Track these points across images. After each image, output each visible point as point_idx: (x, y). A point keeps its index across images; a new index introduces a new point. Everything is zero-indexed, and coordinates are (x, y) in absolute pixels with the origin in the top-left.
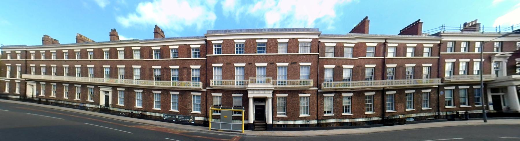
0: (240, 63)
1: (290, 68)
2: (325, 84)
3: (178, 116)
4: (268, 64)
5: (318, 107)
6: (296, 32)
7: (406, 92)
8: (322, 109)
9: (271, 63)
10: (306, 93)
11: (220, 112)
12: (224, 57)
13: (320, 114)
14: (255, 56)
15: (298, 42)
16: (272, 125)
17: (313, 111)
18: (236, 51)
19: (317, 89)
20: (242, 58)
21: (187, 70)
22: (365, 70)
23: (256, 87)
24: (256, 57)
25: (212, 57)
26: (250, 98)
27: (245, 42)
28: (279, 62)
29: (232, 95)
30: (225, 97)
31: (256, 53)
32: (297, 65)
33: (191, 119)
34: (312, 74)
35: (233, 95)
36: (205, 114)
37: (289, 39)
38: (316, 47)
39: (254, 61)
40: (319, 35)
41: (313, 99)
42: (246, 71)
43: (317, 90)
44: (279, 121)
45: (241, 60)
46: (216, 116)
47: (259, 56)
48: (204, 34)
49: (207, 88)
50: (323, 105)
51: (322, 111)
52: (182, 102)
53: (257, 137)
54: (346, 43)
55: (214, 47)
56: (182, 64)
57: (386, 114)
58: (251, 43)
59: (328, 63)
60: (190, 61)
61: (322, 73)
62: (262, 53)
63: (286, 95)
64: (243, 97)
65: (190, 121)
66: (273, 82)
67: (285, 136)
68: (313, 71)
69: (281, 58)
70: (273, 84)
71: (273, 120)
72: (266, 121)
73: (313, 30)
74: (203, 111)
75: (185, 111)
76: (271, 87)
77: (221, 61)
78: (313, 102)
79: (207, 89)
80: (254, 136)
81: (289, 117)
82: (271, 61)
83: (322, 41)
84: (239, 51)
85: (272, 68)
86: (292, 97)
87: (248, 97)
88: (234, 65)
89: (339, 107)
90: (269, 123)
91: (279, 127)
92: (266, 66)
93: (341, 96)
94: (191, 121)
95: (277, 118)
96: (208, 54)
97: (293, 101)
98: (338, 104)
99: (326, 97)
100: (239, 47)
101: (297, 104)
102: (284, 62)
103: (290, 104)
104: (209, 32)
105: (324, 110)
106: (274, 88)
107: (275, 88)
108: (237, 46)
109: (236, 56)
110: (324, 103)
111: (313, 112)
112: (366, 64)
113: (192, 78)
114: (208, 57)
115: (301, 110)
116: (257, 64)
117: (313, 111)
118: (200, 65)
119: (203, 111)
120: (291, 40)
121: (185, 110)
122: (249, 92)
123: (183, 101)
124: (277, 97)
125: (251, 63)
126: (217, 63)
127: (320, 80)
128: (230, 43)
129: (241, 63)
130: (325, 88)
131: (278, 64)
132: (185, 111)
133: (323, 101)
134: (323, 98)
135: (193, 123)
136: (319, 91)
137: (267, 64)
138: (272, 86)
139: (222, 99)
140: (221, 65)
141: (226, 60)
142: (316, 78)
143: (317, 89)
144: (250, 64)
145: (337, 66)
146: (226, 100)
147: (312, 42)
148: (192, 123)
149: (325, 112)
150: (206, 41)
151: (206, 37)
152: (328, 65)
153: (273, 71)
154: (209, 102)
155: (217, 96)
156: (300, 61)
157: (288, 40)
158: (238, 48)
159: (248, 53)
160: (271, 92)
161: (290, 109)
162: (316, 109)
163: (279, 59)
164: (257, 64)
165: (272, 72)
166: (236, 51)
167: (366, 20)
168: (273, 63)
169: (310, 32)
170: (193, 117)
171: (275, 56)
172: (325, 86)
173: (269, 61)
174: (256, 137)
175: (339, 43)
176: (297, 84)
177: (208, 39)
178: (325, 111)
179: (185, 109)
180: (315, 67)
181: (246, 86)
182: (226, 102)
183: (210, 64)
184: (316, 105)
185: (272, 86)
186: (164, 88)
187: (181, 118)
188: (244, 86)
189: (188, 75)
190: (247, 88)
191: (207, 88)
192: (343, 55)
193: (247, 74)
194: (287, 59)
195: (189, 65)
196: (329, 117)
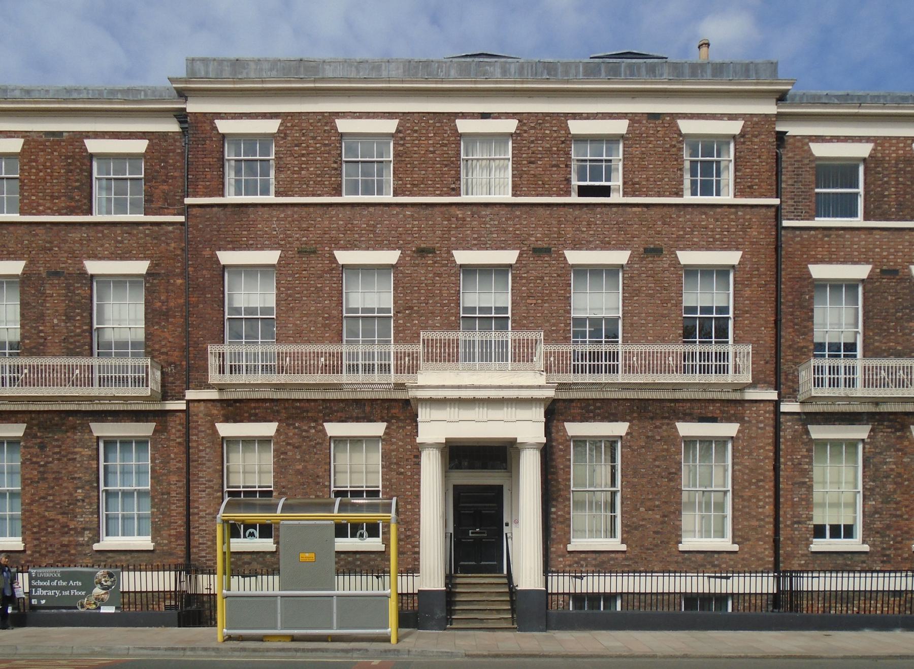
0: (367, 249)
1: (639, 275)
2: (819, 370)
3: (31, 578)
4: (520, 255)
5: (782, 500)
6: (670, 82)
8: (804, 514)
9: (538, 251)
10: (713, 420)
11: (266, 531)
12: (289, 211)
13: (792, 539)
14: (453, 210)
15: (680, 134)
16: (545, 595)
17: (755, 523)
19: (773, 395)
20: (381, 223)
21: (67, 287)
23: (459, 387)
24: (459, 213)
25: (215, 209)
26: (424, 445)
27: (398, 131)
28: (577, 245)
29: (323, 431)
30: (295, 440)
32: (665, 262)
33: (98, 591)
34: (747, 312)
35: (333, 429)
36: (180, 551)
37: (633, 118)
38: (764, 164)
39: (449, 239)
40: (781, 97)
41: (750, 453)
42: (405, 295)
43: (777, 404)
44: (581, 578)
45: (372, 229)
46: (247, 558)
47: (475, 209)
48: (172, 80)
49: (191, 395)
50: (810, 488)
51: (804, 523)
52: (43, 485)
53: (466, 659)
55: (229, 155)
56: (45, 249)
58: (428, 138)
59: (831, 253)
60: (84, 233)
61: (802, 307)
63: (620, 429)
64: (386, 438)
65: (93, 600)
66: (547, 355)
67: (611, 657)
68: (748, 299)
69: (589, 224)
70: (548, 369)
71: (547, 570)
72: (509, 576)
73: (747, 70)
74: (165, 533)
75: (65, 540)
76: (540, 387)
77: (269, 239)
78: (751, 470)
79: (188, 402)
80: (451, 655)
81: (637, 551)
82: (538, 237)
83: (793, 130)
85: (542, 278)
86: (653, 437)
87: (419, 440)
88: (333, 259)
89: (897, 503)
90: (524, 588)
91: (582, 608)
92: (510, 266)
93: (906, 443)
94: (100, 602)
95: (569, 559)
96: (195, 195)
97: (655, 460)
98: (890, 487)
99: (823, 443)
101: (670, 480)
102: (605, 245)
103: (643, 476)
104: (199, 66)
105: (811, 519)
106: (551, 393)
107: (561, 387)
109: (348, 211)
110: (811, 479)
111: (754, 529)
114: (194, 211)
115: (690, 520)
116: (462, 257)
117: (755, 523)
118: (144, 258)
119: (165, 533)
120: (639, 122)
121: (64, 534)
122: (423, 414)
123: (50, 476)
124: (568, 439)
125: (432, 251)
126: (248, 247)
127: (790, 347)
128: (314, 138)
129: (374, 249)
130: (816, 392)
131: (574, 257)
132: (65, 540)
133: (810, 463)
134: (810, 450)
135: (111, 610)
136: (785, 407)
137: (516, 253)
138: (541, 380)
139: (278, 453)
140: (271, 257)
141: (301, 229)
142: (767, 334)
143: (773, 395)
144: (422, 252)
145: (882, 271)
146: (303, 460)
147: (743, 134)
148: (105, 610)
149: (819, 531)
150: (181, 116)
151: (183, 94)
152: (830, 262)
153: (550, 295)
154: (204, 474)
155: (248, 441)
157: (20, 142)
158: (697, 162)
159: (412, 194)
160: (538, 414)
161: (642, 509)
162: (769, 509)
163: (578, 229)
164: (462, 257)
165: (544, 301)
168: (548, 251)
169: (730, 82)
170: (110, 575)
171: (562, 211)
172: (818, 383)
173: (530, 235)
174: (458, 659)
175: (890, 138)
176: (668, 370)
177: (193, 107)
178: (817, 521)
179: (65, 530)
180: (759, 276)
181: (404, 378)
182: (299, 472)
183: (207, 253)
184: (770, 485)
185: (541, 380)
187: (44, 588)
188: (393, 378)
189: (69, 318)
190: (412, 394)
191: (191, 395)
193: (411, 308)
194: (620, 229)
195: (78, 258)
196: (840, 561)
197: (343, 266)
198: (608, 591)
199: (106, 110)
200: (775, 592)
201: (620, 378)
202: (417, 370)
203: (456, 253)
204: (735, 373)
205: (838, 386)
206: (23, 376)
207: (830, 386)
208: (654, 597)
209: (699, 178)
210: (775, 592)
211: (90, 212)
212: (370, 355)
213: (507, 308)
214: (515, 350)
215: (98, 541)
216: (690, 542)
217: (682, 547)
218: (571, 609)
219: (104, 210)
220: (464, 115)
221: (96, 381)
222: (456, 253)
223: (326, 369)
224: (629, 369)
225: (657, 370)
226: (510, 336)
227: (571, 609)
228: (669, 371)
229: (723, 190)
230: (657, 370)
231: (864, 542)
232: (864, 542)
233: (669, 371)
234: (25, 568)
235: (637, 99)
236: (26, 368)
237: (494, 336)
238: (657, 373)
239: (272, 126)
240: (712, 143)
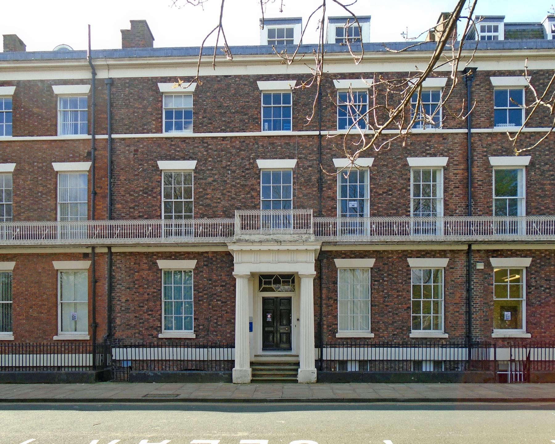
37: (299, 78)
54: (173, 79)
102: (283, 157)
107: (323, 244)
157: (293, 83)
198: (416, 359)
199: (49, 67)
200: (467, 359)
202: (233, 234)
203: (54, 164)
204: (445, 234)
206: (17, 233)
208: (202, 363)
210: (467, 359)
211: (56, 135)
212: (180, 226)
214: (289, 222)
215: (57, 334)
218: (443, 370)
219: (289, 128)
220: (343, 76)
221: (183, 233)
222: (54, 164)
223: (151, 236)
225: (141, 236)
226: (292, 212)
227: (443, 370)
230: (141, 236)
231: (445, 332)
232: (445, 332)
234: (547, 346)
235: (82, 71)
237: (281, 213)
238: (141, 237)
239: (365, 84)
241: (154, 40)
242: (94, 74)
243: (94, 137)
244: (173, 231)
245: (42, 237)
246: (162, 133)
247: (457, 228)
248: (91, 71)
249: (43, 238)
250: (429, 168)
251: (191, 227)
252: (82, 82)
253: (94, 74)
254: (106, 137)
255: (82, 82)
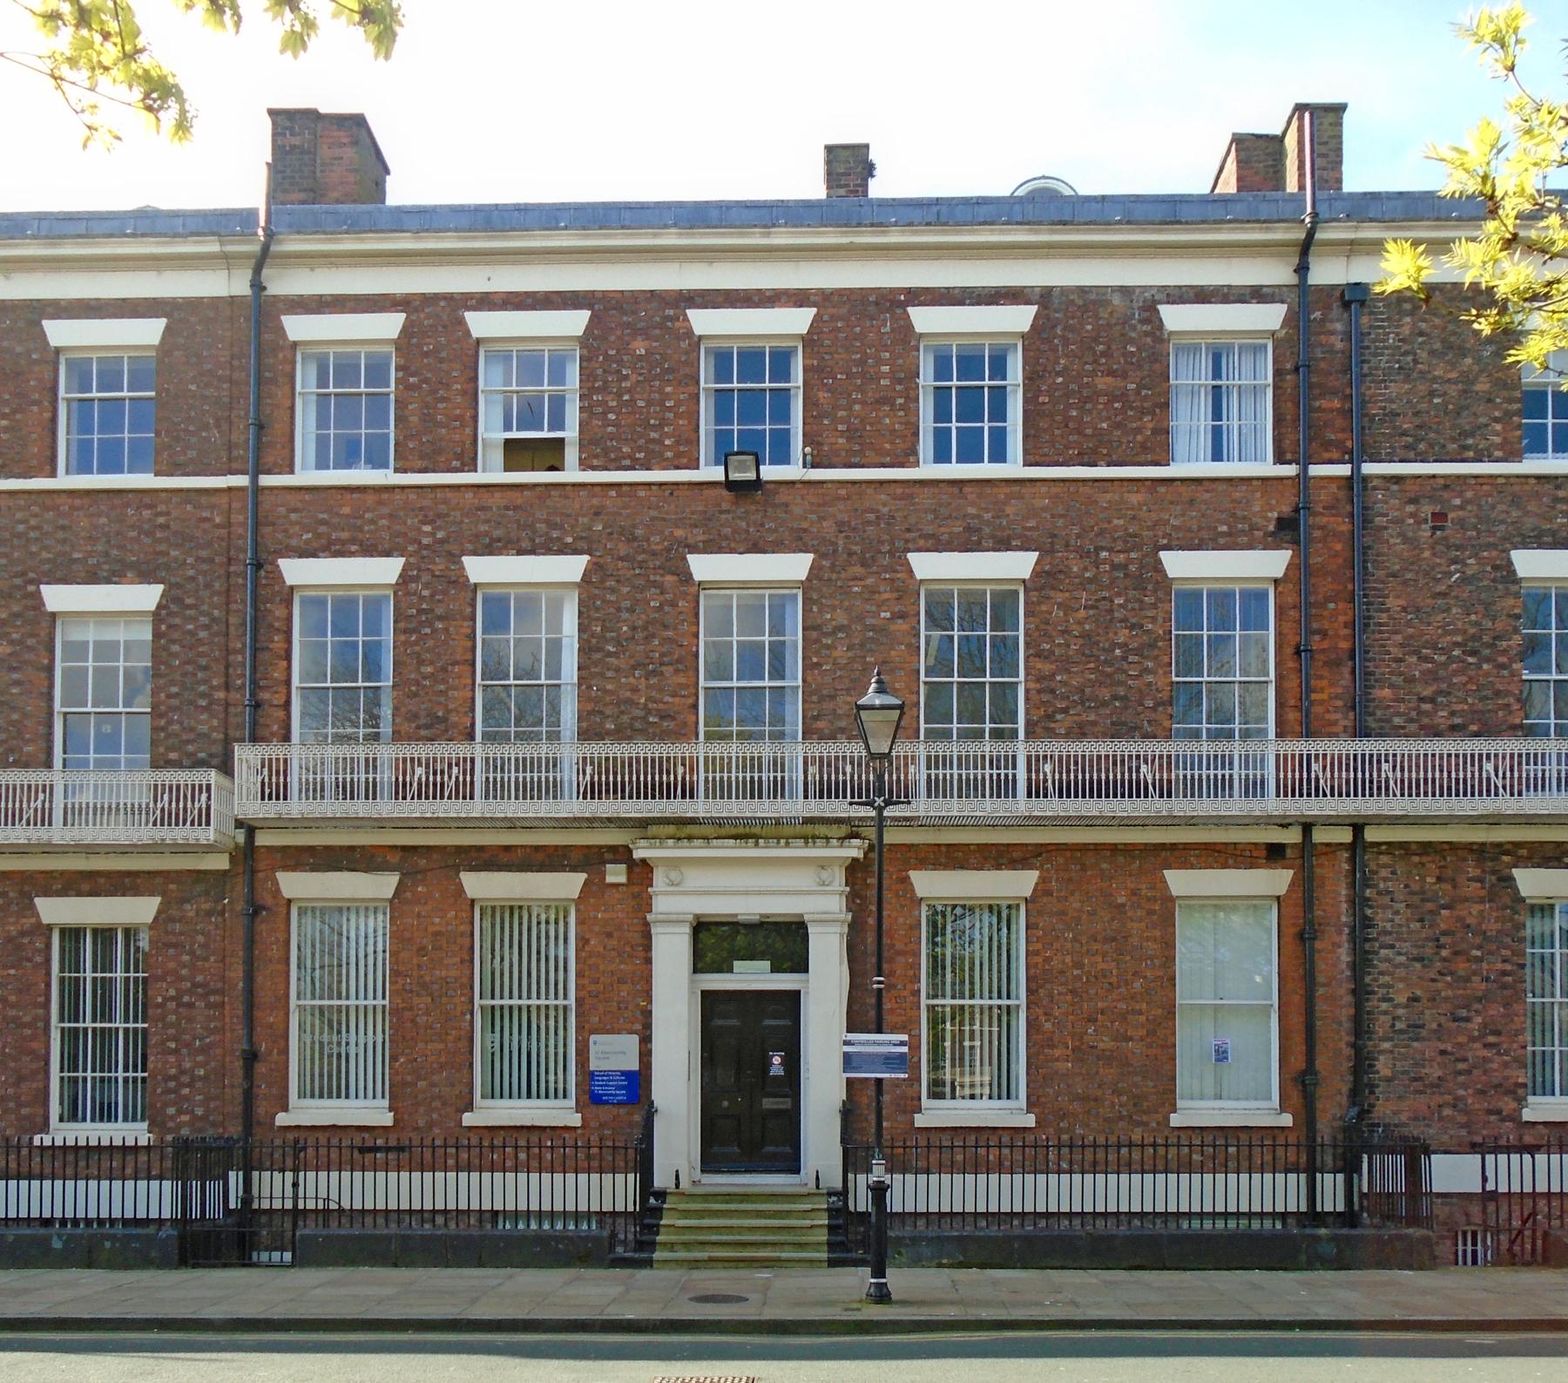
7: (54, 910)
18: (706, 425)
22: (73, 642)
31: (695, 465)
37: (1044, 297)
54: (1202, 295)
57: (1479, 1157)
62: (118, 469)
84: (954, 425)
100: (767, 385)
108: (722, 360)
112: (1168, 548)
113: (55, 1036)
156: (910, 546)
166: (706, 425)
167: (60, 23)
186: (921, 1303)
192: (1164, 432)
197: (700, 583)
201: (477, 808)
203: (914, 558)
205: (692, 797)
207: (707, 797)
209: (986, 426)
213: (783, 678)
215: (285, 1109)
216: (1193, 1111)
217: (1175, 1120)
220: (486, 302)
222: (914, 558)
224: (494, 790)
228: (1488, 791)
229: (1180, 445)
233: (1488, 791)
236: (420, 765)
240: (1218, 353)
241: (387, 172)
242: (1302, 269)
243: (254, 480)
244: (1236, 777)
245: (446, 794)
246: (53, 474)
247: (1426, 772)
248: (1296, 261)
249: (413, 798)
250: (1548, 584)
251: (1543, 764)
252: (1257, 295)
253: (1302, 269)
254: (242, 481)
255: (1257, 295)
